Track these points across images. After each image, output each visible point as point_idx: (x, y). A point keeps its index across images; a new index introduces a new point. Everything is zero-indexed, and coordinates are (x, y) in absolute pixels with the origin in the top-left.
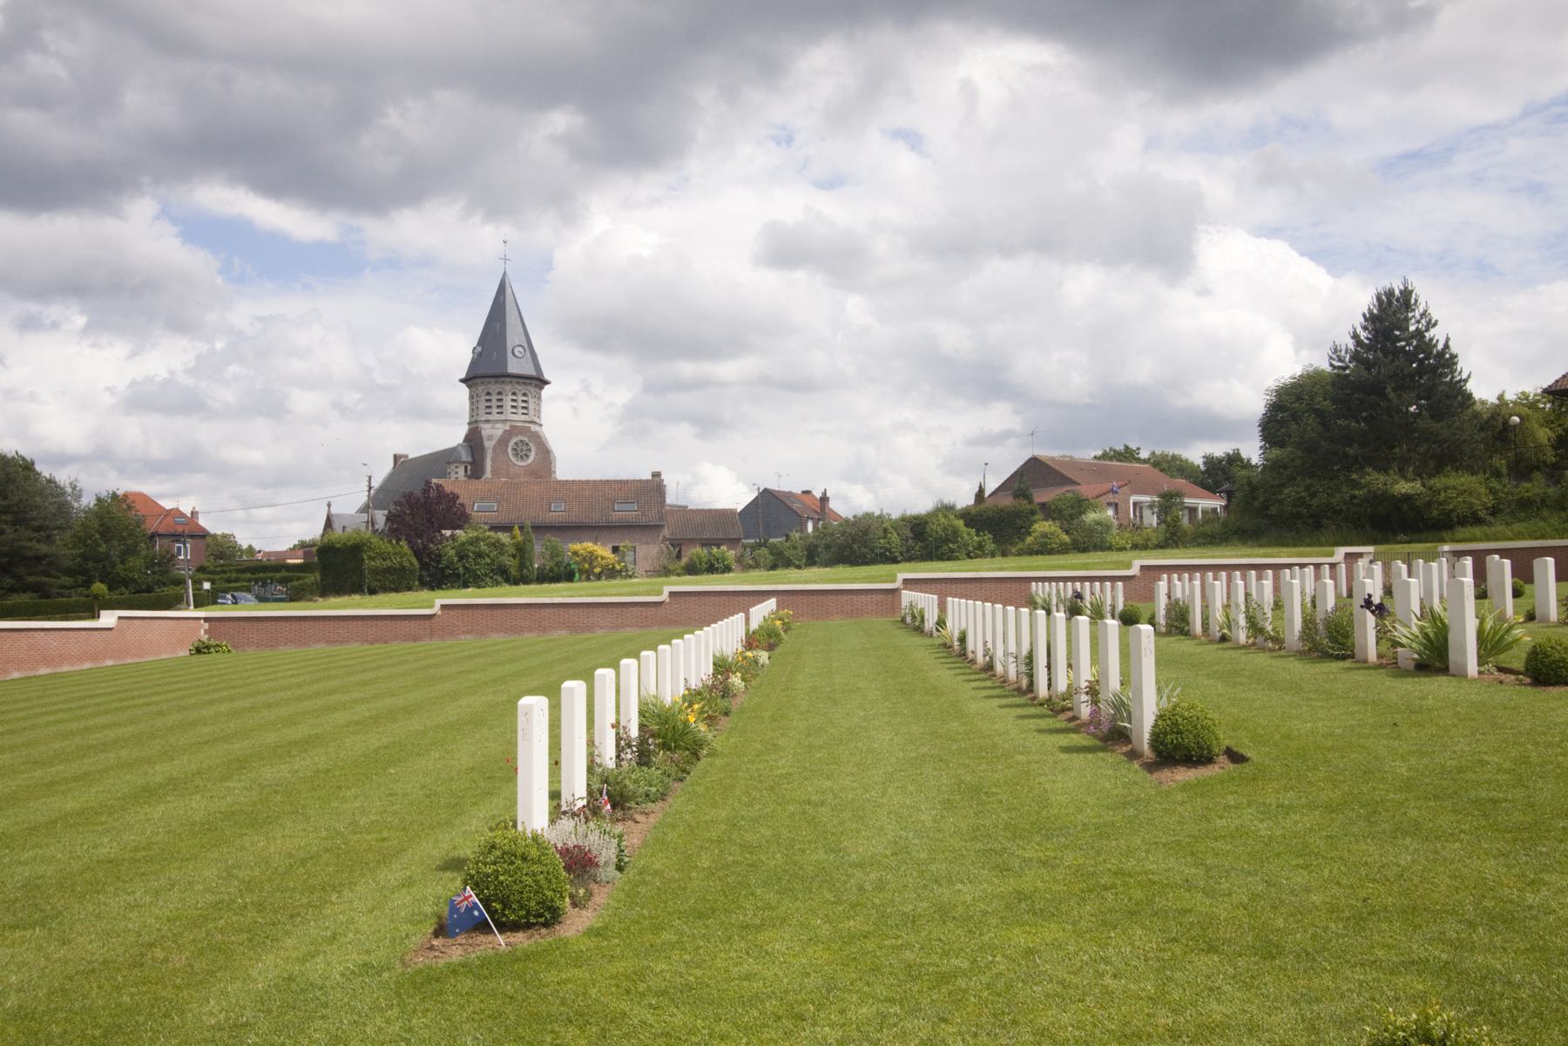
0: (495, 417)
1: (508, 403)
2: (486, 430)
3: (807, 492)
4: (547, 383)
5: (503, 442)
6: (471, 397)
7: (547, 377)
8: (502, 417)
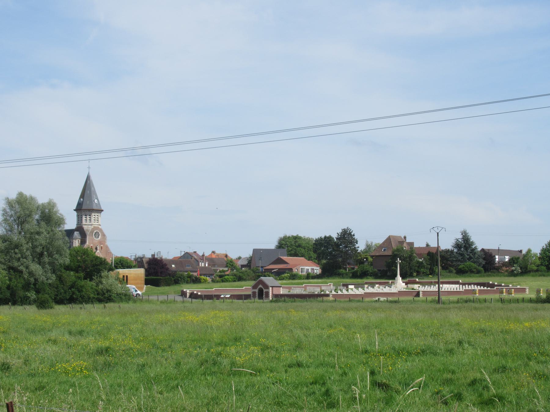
0: (88, 223)
1: (93, 219)
2: (85, 227)
3: (195, 252)
4: (102, 211)
5: (92, 232)
6: (78, 216)
7: (102, 209)
8: (91, 223)
